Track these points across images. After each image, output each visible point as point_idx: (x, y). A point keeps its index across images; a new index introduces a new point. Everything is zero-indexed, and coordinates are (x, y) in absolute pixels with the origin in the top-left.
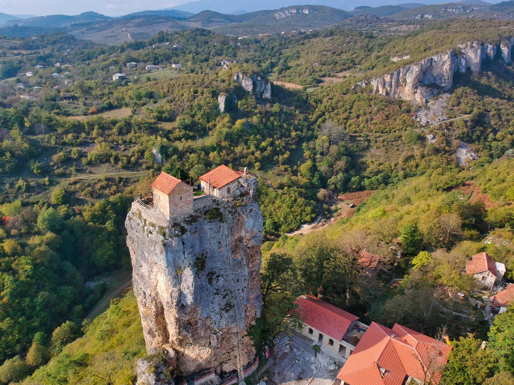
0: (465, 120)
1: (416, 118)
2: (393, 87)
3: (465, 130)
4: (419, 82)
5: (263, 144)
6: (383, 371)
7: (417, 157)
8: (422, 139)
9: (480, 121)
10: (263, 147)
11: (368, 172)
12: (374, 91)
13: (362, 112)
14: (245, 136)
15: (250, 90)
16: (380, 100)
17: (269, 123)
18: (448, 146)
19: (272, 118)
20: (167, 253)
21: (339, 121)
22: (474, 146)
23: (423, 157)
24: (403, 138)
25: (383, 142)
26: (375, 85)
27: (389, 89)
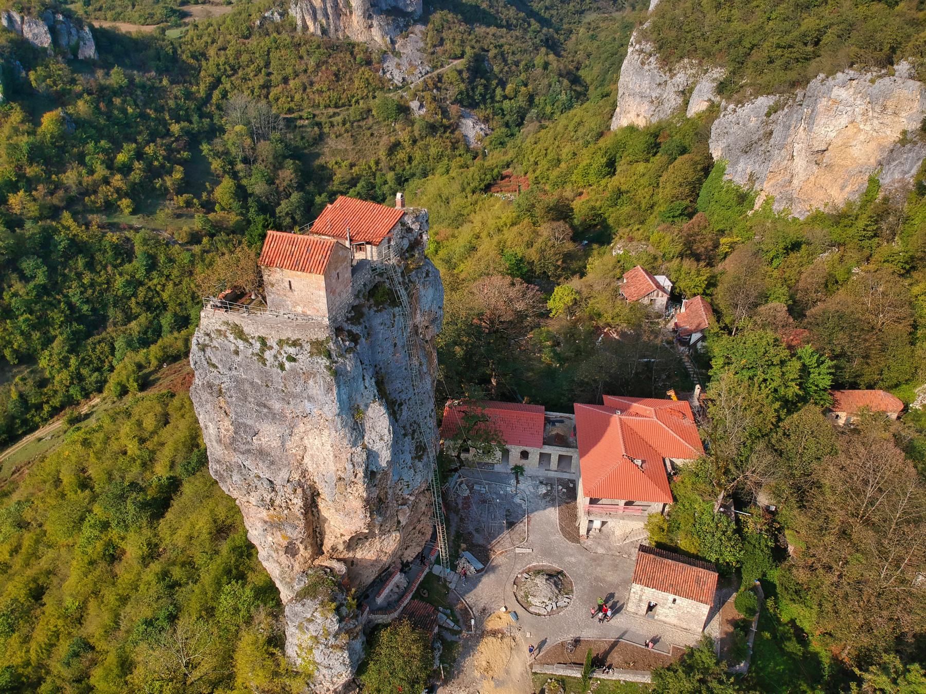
0: (458, 68)
1: (384, 73)
2: (331, 17)
3: (462, 86)
4: (372, 6)
5: (121, 158)
6: (639, 462)
7: (406, 144)
8: (403, 110)
9: (478, 68)
10: (124, 164)
11: (336, 182)
12: (299, 28)
13: (289, 70)
14: (74, 146)
15: (46, 45)
16: (315, 44)
17: (116, 112)
18: (445, 117)
19: (117, 101)
20: (339, 387)
21: (252, 92)
22: (480, 113)
23: (415, 142)
24: (374, 112)
25: (344, 124)
26: (298, 17)
27: (324, 21)
